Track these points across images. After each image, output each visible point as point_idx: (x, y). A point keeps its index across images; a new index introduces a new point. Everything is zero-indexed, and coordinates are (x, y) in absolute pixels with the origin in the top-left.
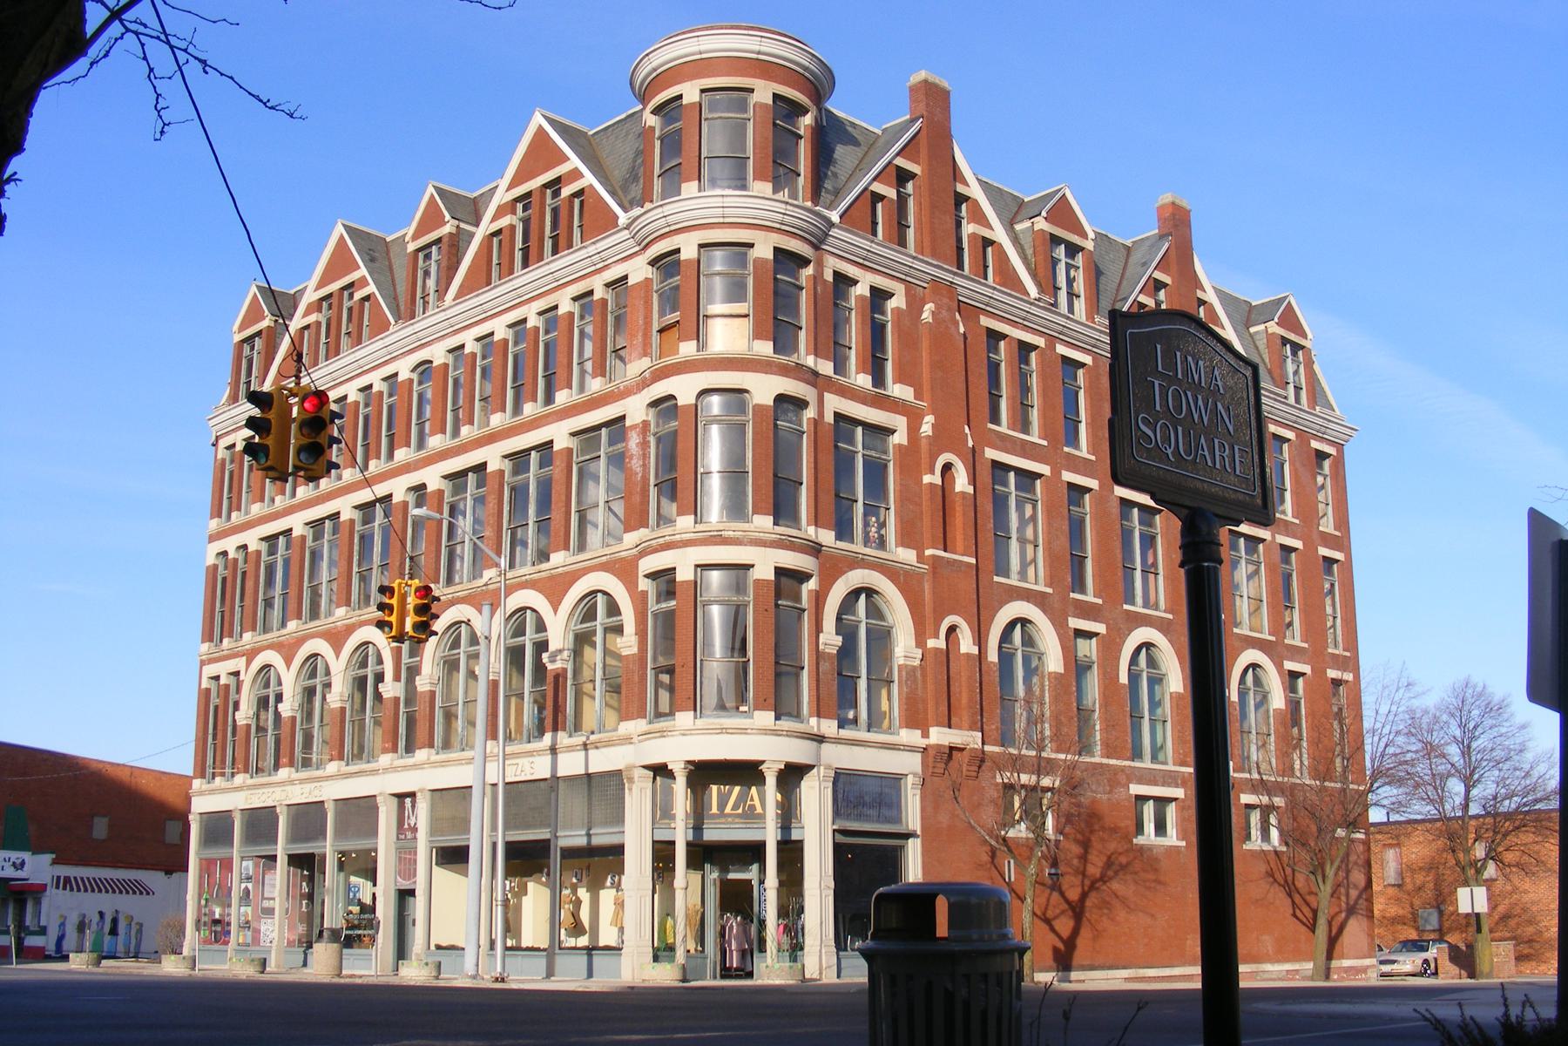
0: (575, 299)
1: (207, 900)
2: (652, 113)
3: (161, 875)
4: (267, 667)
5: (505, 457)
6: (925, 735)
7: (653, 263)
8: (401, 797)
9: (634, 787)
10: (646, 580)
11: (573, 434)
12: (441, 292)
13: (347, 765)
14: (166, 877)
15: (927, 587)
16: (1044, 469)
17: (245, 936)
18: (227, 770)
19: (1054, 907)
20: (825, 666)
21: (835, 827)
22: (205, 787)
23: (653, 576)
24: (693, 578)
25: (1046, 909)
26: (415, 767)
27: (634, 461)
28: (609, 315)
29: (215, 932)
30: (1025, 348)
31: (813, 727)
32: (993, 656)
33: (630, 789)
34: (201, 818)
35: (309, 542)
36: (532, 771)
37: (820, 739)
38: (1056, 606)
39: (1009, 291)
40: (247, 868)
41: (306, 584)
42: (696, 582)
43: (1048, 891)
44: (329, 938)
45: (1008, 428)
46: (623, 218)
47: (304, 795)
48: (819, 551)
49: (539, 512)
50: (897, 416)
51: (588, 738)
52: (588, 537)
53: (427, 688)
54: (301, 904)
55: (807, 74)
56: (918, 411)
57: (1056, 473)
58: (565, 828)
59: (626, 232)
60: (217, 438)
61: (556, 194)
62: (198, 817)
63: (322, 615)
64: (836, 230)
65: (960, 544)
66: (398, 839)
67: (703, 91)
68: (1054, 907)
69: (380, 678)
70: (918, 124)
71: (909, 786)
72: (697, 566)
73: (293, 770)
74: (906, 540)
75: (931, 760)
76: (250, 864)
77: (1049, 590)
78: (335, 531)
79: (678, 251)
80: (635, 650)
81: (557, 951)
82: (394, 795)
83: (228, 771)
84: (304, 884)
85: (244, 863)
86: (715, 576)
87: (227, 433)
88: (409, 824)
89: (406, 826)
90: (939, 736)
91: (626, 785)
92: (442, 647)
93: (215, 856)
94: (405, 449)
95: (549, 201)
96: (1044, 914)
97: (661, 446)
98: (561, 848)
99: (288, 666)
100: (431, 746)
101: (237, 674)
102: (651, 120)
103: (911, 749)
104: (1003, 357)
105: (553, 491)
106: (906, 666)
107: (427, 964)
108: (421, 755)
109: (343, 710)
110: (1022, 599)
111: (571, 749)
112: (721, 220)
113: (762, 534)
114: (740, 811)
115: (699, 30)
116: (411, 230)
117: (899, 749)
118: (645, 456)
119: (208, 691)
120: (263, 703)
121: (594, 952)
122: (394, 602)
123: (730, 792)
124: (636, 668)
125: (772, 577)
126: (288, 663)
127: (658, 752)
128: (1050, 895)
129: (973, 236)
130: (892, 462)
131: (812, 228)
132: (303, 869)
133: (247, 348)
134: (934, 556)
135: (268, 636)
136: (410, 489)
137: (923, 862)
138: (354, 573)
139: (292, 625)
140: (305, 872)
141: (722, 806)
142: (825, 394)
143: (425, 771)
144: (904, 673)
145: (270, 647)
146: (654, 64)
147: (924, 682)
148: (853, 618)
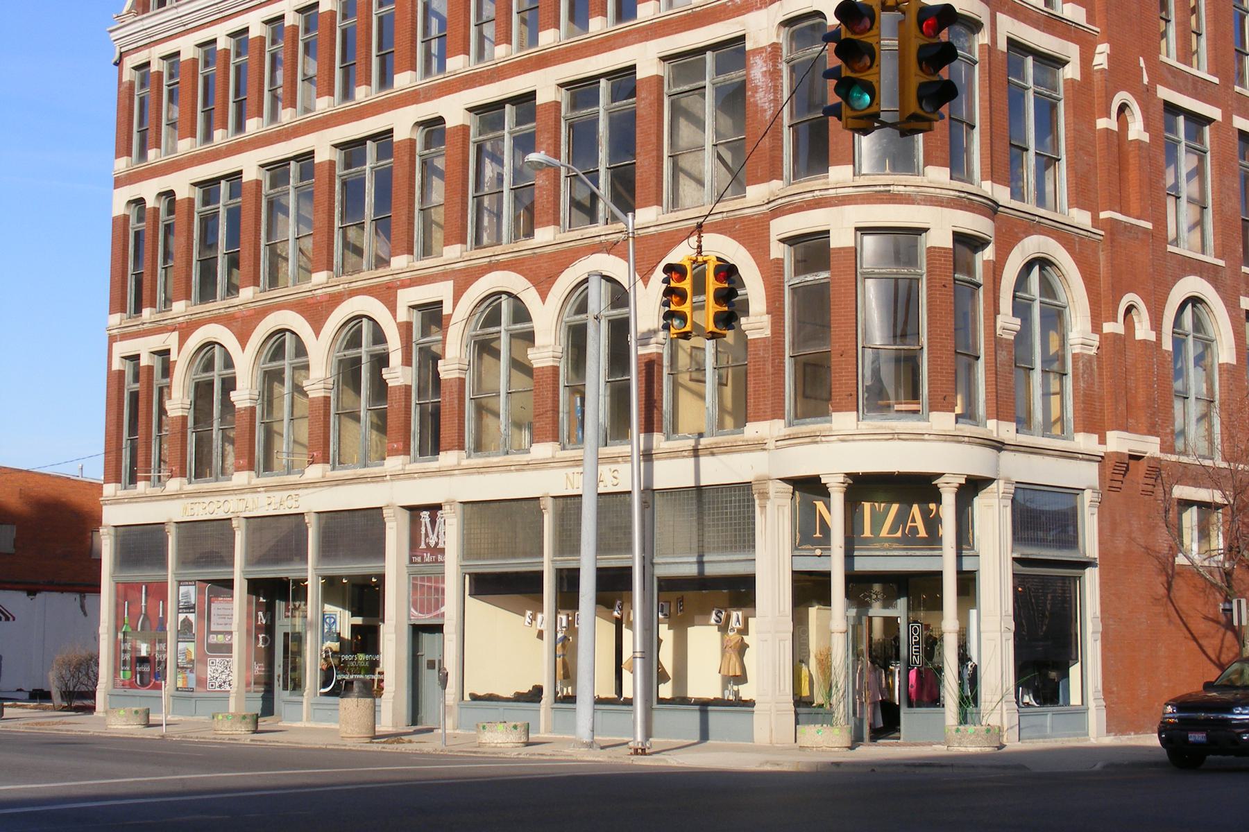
3: (22, 596)
4: (211, 344)
5: (561, 85)
6: (1102, 441)
8: (414, 510)
9: (769, 505)
11: (664, 59)
13: (333, 469)
14: (28, 599)
15: (1102, 257)
16: (1214, 113)
17: (185, 679)
18: (152, 474)
19: (1228, 649)
20: (1003, 355)
21: (1015, 555)
23: (790, 241)
24: (853, 245)
25: (1220, 652)
26: (440, 473)
27: (760, 95)
29: (141, 673)
31: (992, 431)
32: (1167, 345)
33: (763, 507)
34: (116, 532)
36: (615, 482)
38: (1228, 282)
40: (187, 595)
42: (856, 249)
43: (1223, 630)
44: (360, 691)
45: (1178, 60)
47: (273, 506)
48: (995, 212)
50: (1070, 43)
51: (697, 443)
53: (456, 375)
54: (257, 638)
57: (1227, 117)
58: (663, 555)
62: (112, 531)
63: (290, 283)
65: (1135, 205)
66: (411, 561)
68: (1228, 649)
69: (381, 361)
71: (1087, 503)
72: (857, 229)
74: (1081, 198)
75: (1108, 472)
76: (192, 590)
77: (1221, 263)
80: (767, 333)
81: (655, 705)
82: (461, 503)
83: (154, 474)
84: (260, 614)
85: (183, 589)
86: (869, 241)
87: (137, 49)
88: (427, 544)
89: (423, 546)
90: (1118, 442)
91: (757, 502)
93: (137, 579)
94: (409, 73)
96: (1218, 658)
99: (243, 346)
100: (461, 447)
101: (165, 353)
103: (1089, 457)
105: (638, 130)
106: (1083, 355)
107: (515, 727)
108: (448, 458)
109: (327, 400)
110: (1195, 274)
111: (673, 454)
113: (938, 191)
114: (899, 534)
117: (1077, 458)
118: (776, 89)
119: (121, 373)
120: (202, 391)
121: (710, 708)
123: (887, 512)
127: (804, 462)
128: (1224, 634)
132: (258, 596)
134: (1111, 220)
135: (210, 306)
137: (1101, 597)
138: (336, 229)
139: (247, 293)
140: (262, 599)
142: (998, 14)
143: (454, 478)
144: (1081, 364)
145: (215, 319)
147: (1100, 375)
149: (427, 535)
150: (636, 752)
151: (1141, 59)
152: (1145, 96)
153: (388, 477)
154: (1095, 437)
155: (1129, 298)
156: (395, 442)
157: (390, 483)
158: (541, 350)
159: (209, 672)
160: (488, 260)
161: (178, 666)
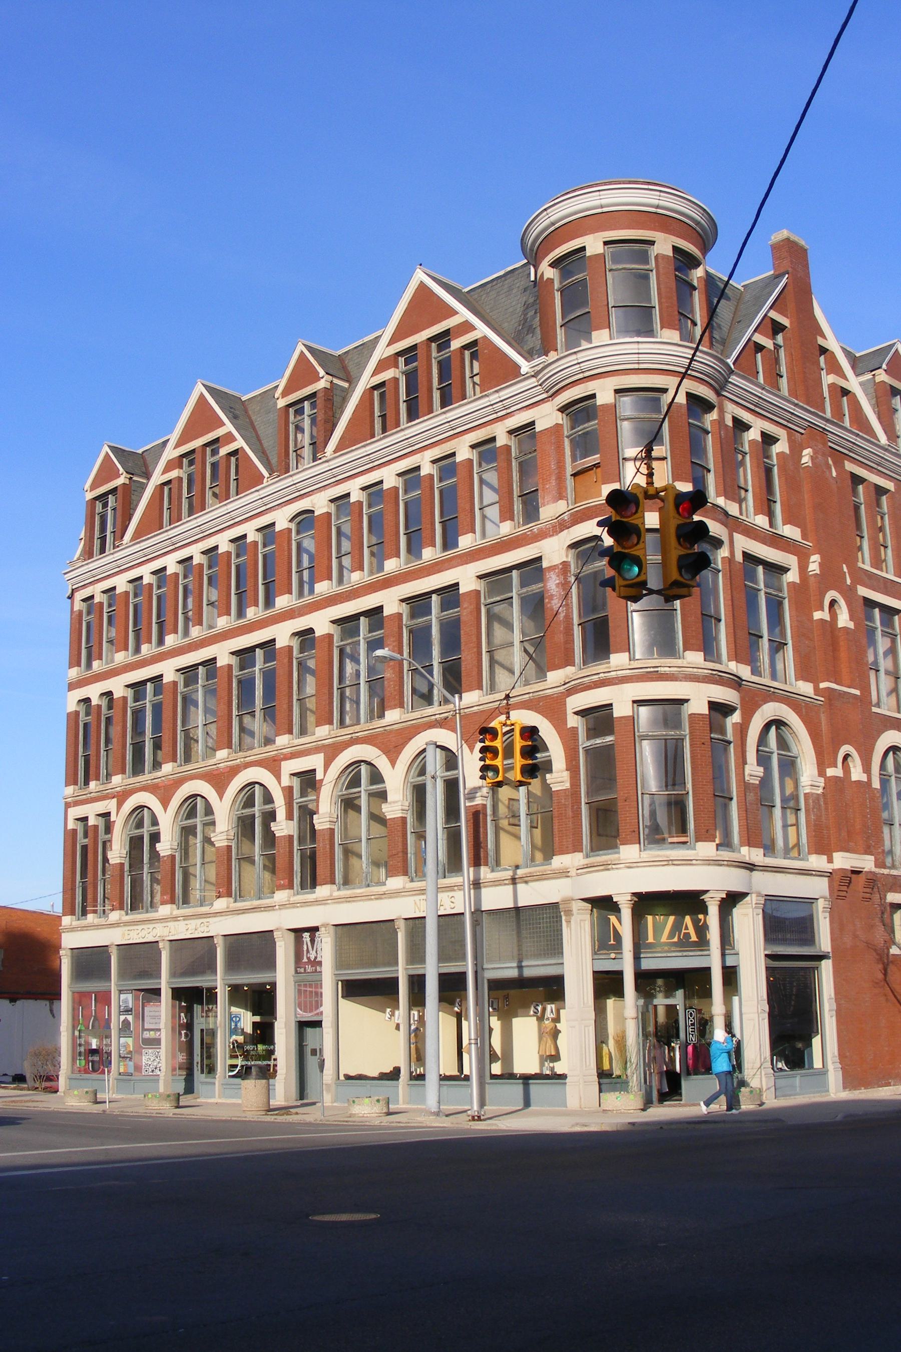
0: (473, 447)
1: (80, 1031)
2: (550, 265)
4: (141, 807)
5: (402, 601)
6: (830, 860)
7: (562, 410)
8: (298, 932)
9: (573, 919)
10: (576, 716)
11: (480, 577)
12: (317, 447)
13: (235, 901)
15: (823, 718)
18: (98, 908)
21: (767, 952)
22: (76, 923)
23: (582, 713)
24: (631, 714)
26: (317, 902)
28: (513, 460)
29: (93, 1062)
30: (880, 491)
31: (745, 856)
33: (568, 922)
34: (72, 953)
35: (181, 688)
36: (453, 905)
37: (751, 867)
39: (869, 438)
40: (126, 1001)
41: (179, 728)
44: (257, 1075)
46: (525, 367)
48: (740, 685)
49: (444, 652)
51: (515, 873)
52: (496, 677)
54: (180, 1034)
55: (698, 229)
56: (805, 551)
58: (490, 961)
59: (534, 379)
60: (72, 594)
61: (215, 452)
62: (69, 952)
64: (734, 377)
66: (296, 972)
67: (606, 243)
69: (270, 816)
70: (784, 280)
72: (634, 702)
73: (174, 906)
74: (804, 673)
75: (836, 884)
76: (129, 997)
78: (211, 675)
79: (593, 396)
80: (567, 785)
83: (100, 908)
84: (183, 1015)
85: (123, 996)
87: (84, 586)
88: (308, 958)
89: (305, 960)
90: (842, 861)
91: (564, 918)
92: (340, 786)
95: (434, 354)
97: (580, 585)
98: (488, 980)
100: (333, 882)
101: (107, 815)
102: (549, 273)
103: (820, 874)
104: (862, 500)
106: (813, 794)
107: (378, 1101)
108: (323, 891)
110: (894, 729)
112: (636, 366)
113: (695, 670)
114: (676, 939)
115: (597, 185)
116: (283, 383)
117: (811, 875)
119: (74, 831)
120: (135, 843)
121: (531, 1081)
122: (498, 744)
124: (569, 802)
125: (706, 711)
126: (165, 804)
129: (832, 386)
130: (787, 600)
131: (717, 375)
132: (180, 1001)
133: (99, 506)
136: (295, 634)
138: (234, 717)
140: (183, 1004)
141: (658, 931)
143: (328, 906)
145: (144, 789)
146: (552, 219)
147: (826, 809)
148: (767, 749)
149: (308, 951)
150: (473, 1119)
151: (844, 566)
152: (849, 594)
153: (277, 907)
154: (825, 857)
155: (845, 749)
156: (282, 880)
157: (279, 912)
158: (393, 805)
159: (144, 1061)
160: (350, 736)
161: (120, 1057)
